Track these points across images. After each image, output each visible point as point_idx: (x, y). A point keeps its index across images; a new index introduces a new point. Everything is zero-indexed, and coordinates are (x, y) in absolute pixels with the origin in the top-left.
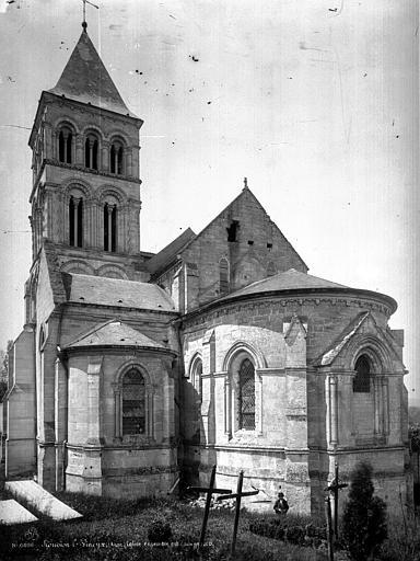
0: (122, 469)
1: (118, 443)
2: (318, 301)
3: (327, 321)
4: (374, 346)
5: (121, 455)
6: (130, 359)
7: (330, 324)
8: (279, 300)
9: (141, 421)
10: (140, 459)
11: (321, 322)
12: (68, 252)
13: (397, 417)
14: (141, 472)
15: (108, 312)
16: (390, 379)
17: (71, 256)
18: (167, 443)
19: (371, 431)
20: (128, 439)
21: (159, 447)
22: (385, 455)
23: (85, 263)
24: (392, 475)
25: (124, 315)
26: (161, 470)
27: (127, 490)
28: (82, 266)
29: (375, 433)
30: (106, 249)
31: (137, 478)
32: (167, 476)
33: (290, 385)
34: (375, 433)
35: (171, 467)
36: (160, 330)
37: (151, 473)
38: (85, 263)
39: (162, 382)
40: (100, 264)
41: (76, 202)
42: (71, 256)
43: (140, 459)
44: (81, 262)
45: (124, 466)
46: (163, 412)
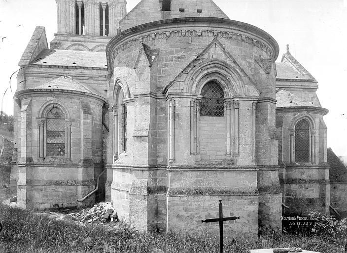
0: (43, 180)
1: (41, 161)
2: (168, 34)
3: (177, 52)
4: (222, 71)
5: (43, 170)
6: (50, 99)
7: (180, 54)
8: (136, 37)
9: (62, 147)
10: (59, 174)
11: (171, 53)
12: (72, 38)
13: (249, 140)
14: (57, 183)
15: (59, 71)
16: (241, 103)
17: (73, 41)
18: (81, 163)
19: (223, 153)
20: (49, 159)
21: (76, 166)
22: (233, 174)
23: (83, 45)
24: (241, 194)
25: (72, 72)
26: (76, 183)
27: (47, 196)
28: (81, 47)
29: (226, 154)
30: (101, 34)
31: (54, 187)
32: (80, 188)
33: (137, 110)
34: (226, 154)
35: (83, 181)
36: (103, 82)
37: (66, 185)
38: (83, 45)
39: (79, 117)
40: (94, 45)
41: (104, 7)
42: (73, 41)
43: (59, 174)
44: (79, 45)
45: (45, 179)
46: (80, 140)
